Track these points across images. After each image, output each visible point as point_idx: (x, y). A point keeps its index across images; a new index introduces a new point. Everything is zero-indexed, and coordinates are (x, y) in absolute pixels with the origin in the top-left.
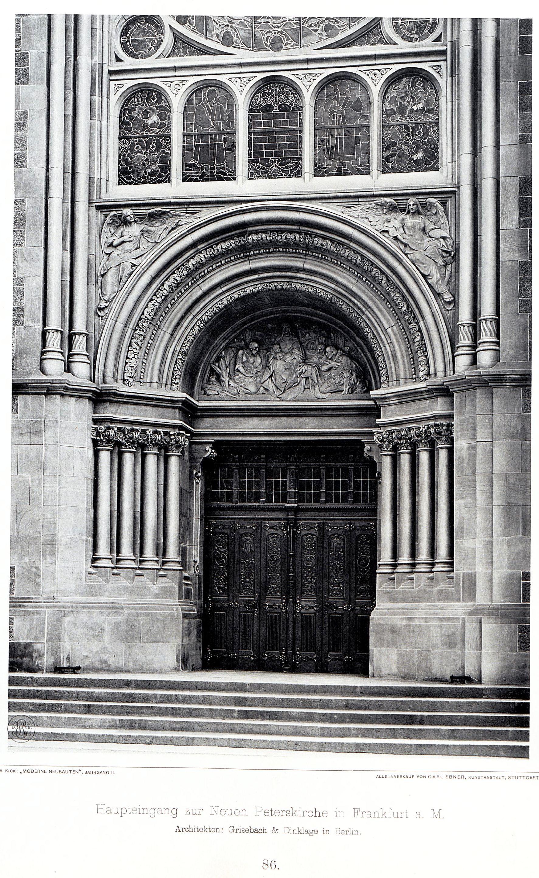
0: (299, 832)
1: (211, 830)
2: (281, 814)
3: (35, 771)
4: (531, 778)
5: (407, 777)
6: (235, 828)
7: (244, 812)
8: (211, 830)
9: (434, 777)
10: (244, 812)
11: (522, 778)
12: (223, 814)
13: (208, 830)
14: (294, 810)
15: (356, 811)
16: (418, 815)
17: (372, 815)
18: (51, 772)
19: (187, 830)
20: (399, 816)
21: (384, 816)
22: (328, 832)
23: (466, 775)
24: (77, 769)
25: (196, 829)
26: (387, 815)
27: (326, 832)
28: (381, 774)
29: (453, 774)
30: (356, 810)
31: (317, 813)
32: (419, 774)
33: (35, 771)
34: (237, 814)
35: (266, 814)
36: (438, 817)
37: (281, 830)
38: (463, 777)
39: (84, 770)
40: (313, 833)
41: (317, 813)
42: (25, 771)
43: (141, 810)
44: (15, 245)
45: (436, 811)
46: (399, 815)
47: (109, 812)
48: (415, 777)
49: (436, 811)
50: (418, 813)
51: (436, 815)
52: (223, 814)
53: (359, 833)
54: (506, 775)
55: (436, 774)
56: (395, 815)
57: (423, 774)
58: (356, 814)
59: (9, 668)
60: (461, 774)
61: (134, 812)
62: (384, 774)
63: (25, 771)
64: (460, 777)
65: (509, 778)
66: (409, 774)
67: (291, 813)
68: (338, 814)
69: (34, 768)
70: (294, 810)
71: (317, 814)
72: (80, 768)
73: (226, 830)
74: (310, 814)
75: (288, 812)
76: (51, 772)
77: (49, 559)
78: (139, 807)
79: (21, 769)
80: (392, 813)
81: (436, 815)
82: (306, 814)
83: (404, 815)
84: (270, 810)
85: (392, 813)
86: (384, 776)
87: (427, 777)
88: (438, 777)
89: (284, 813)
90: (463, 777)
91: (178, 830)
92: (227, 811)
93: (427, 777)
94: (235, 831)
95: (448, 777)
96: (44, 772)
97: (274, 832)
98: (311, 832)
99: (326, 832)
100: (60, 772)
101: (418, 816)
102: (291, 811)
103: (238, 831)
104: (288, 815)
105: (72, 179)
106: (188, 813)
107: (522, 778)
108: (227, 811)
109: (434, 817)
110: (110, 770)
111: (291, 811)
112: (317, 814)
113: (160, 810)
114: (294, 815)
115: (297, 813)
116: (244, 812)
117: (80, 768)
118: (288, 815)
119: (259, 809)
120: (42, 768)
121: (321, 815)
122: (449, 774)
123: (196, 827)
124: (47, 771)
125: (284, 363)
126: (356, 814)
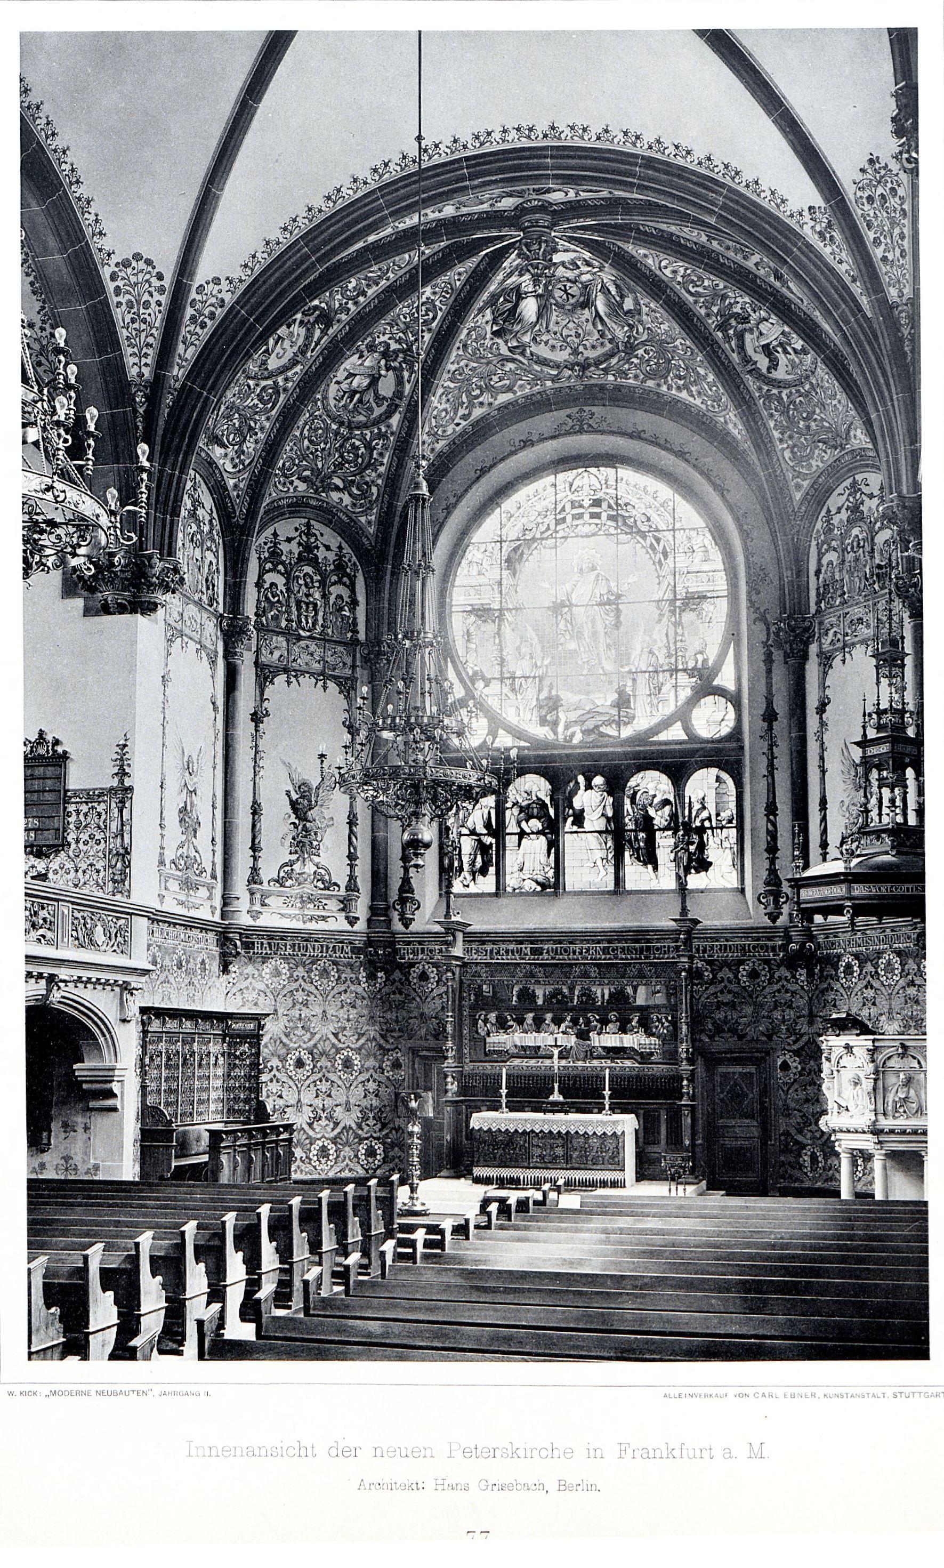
2: (492, 1454)
5: (717, 1396)
9: (764, 1395)
11: (917, 1395)
13: (414, 1486)
16: (728, 1453)
23: (780, 1392)
24: (145, 1388)
29: (796, 1391)
31: (303, 1450)
38: (813, 1395)
41: (303, 1450)
44: (35, 850)
45: (756, 1447)
46: (698, 1455)
49: (756, 1447)
59: (29, 1230)
60: (809, 1391)
61: (226, 1454)
63: (54, 1393)
66: (721, 1391)
68: (592, 1452)
71: (303, 1452)
72: (150, 1386)
74: (544, 1453)
77: (80, 1135)
79: (46, 1390)
81: (756, 1453)
82: (535, 1453)
83: (706, 1454)
89: (498, 1453)
90: (813, 1395)
93: (751, 1396)
103: (495, 1488)
107: (917, 1395)
112: (556, 1453)
117: (150, 1386)
122: (789, 1391)
124: (93, 1393)
125: (647, 638)
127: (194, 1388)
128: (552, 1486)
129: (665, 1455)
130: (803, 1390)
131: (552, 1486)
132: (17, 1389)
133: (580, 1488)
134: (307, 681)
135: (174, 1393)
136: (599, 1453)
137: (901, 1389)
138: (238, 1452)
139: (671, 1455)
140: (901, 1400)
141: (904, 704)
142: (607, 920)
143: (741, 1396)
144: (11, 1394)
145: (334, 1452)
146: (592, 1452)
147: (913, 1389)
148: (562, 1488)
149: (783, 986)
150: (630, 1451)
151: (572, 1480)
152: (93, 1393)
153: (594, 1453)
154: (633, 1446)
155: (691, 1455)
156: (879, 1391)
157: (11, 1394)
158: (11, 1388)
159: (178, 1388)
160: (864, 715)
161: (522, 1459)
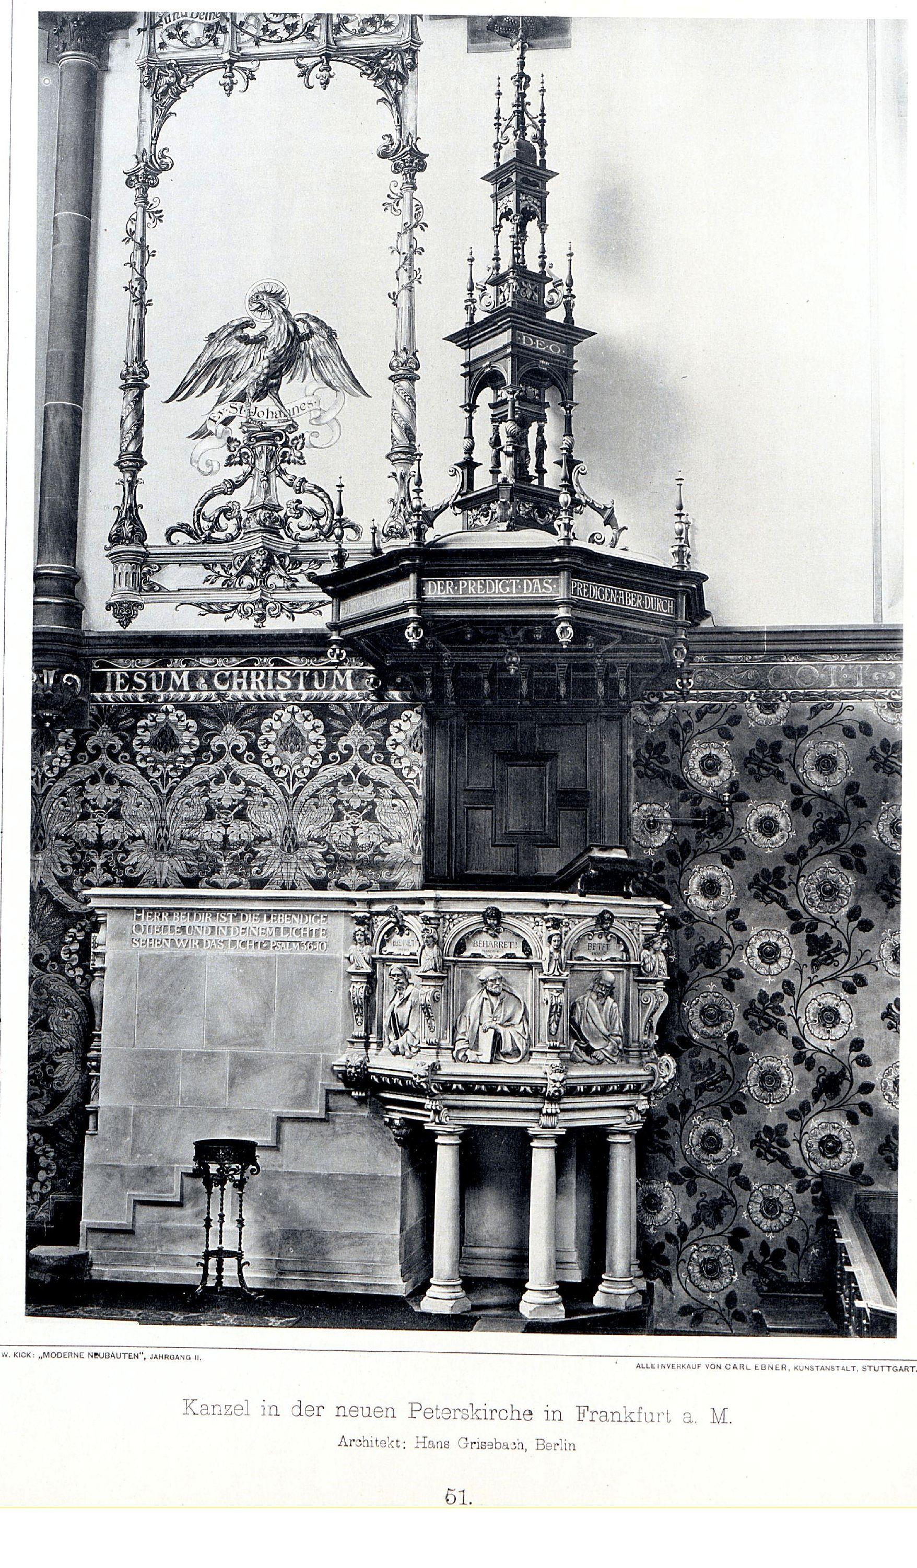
2: (316, 1412)
5: (689, 1366)
6: (469, 1441)
10: (390, 1411)
12: (378, 1415)
13: (394, 1444)
15: (582, 1411)
17: (210, 1410)
20: (551, 1417)
21: (628, 1419)
23: (751, 1363)
24: (136, 1351)
26: (635, 1417)
28: (643, 1361)
29: (767, 1362)
30: (583, 1411)
31: (516, 1413)
34: (310, 1413)
38: (784, 1367)
39: (148, 1353)
42: (46, 1355)
43: (489, 1413)
45: (719, 1412)
46: (489, 1416)
47: (204, 1412)
48: (703, 1367)
49: (719, 1412)
50: (687, 1415)
51: (720, 1418)
55: (738, 1362)
56: (649, 1418)
58: (582, 1415)
60: (780, 1362)
61: (238, 1412)
62: (650, 1361)
63: (46, 1355)
65: (864, 1369)
67: (470, 1413)
69: (62, 1350)
72: (141, 1350)
75: (465, 1412)
78: (485, 1407)
79: (39, 1351)
80: (642, 1416)
81: (720, 1418)
86: (649, 1366)
87: (193, 1358)
91: (343, 1444)
92: (360, 1410)
93: (193, 1358)
94: (469, 1446)
95: (760, 1368)
103: (475, 1446)
106: (229, 1412)
108: (360, 1410)
113: (604, 1414)
116: (390, 1411)
117: (141, 1350)
121: (371, 1414)
122: (759, 1363)
124: (85, 1355)
126: (582, 1415)
128: (531, 1445)
129: (623, 1418)
130: (774, 1363)
131: (531, 1445)
132: (11, 1351)
134: (139, 475)
136: (557, 1415)
137: (870, 1363)
138: (366, 1411)
139: (629, 1418)
140: (870, 1374)
141: (543, 265)
143: (712, 1367)
144: (5, 1355)
145: (297, 1411)
146: (551, 1414)
147: (870, 1363)
149: (228, 768)
150: (588, 1415)
151: (551, 1439)
152: (85, 1355)
153: (556, 1416)
155: (649, 1419)
156: (849, 1364)
159: (169, 1352)
160: (471, 289)
161: (515, 1421)
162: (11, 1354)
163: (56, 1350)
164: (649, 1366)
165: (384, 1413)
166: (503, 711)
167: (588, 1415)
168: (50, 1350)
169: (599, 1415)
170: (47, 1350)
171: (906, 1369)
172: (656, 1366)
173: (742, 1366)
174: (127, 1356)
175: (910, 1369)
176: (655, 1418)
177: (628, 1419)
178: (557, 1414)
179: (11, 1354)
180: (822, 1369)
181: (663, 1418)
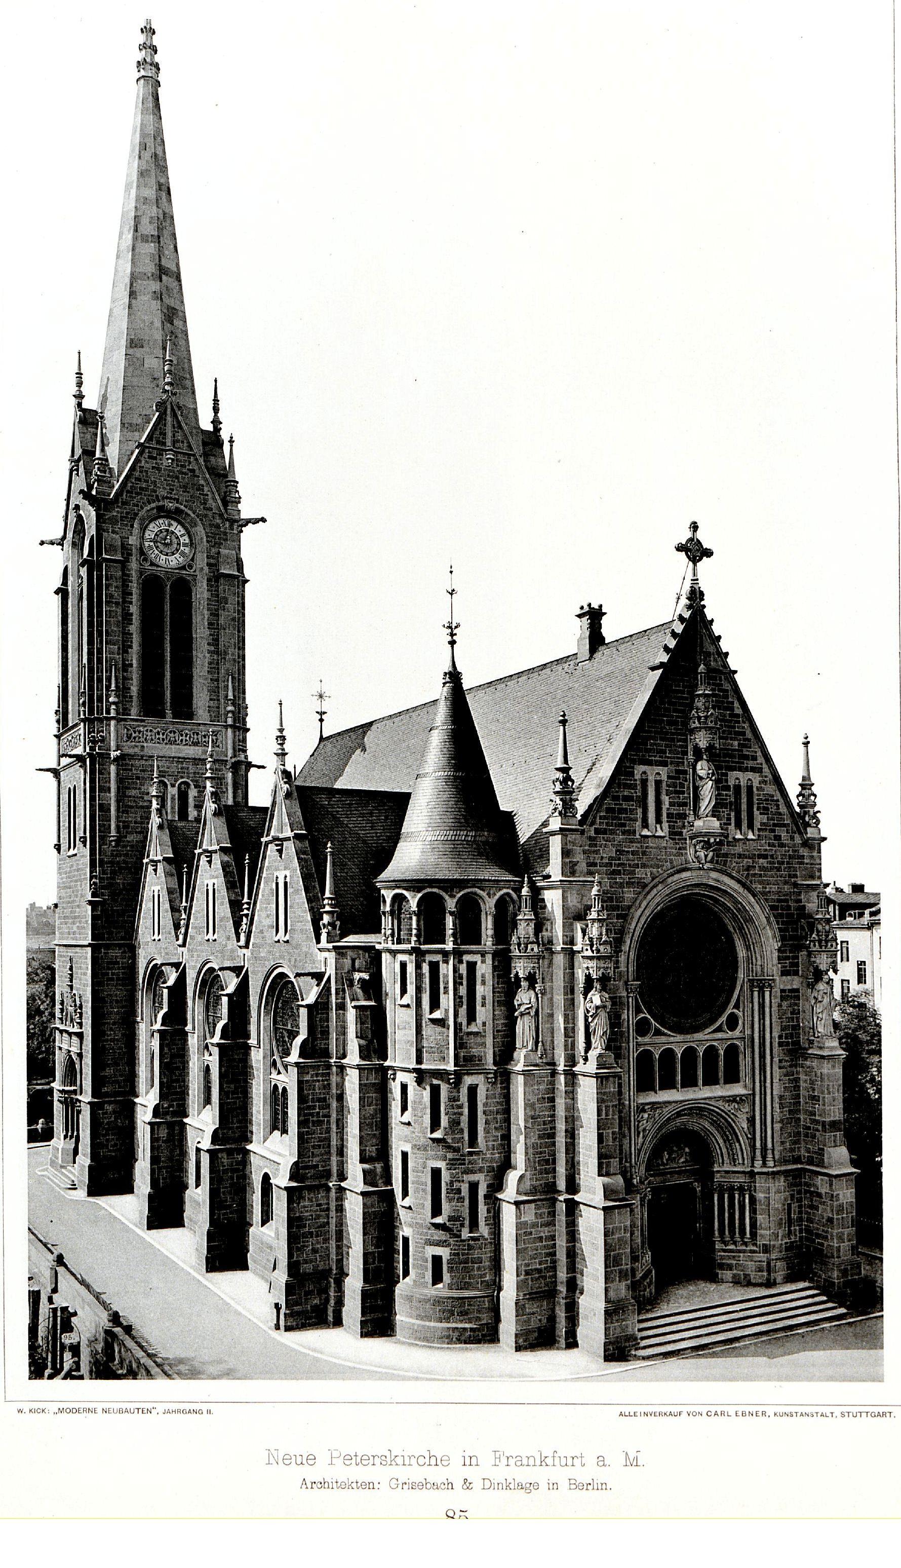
0: (508, 1487)
1: (359, 1484)
3: (78, 1411)
4: (879, 1414)
6: (400, 1482)
7: (311, 1459)
8: (359, 1484)
11: (864, 1415)
13: (354, 1485)
14: (394, 1454)
15: (497, 1456)
18: (105, 1411)
19: (319, 1486)
20: (468, 1463)
21: (393, 1463)
22: (604, 1486)
23: (770, 1411)
25: (335, 1484)
26: (549, 1461)
27: (554, 1486)
28: (626, 1409)
29: (747, 1409)
31: (433, 1459)
32: (691, 1409)
33: (78, 1411)
35: (347, 1462)
36: (635, 1463)
37: (477, 1484)
38: (764, 1413)
39: (161, 1408)
40: (532, 1488)
42: (61, 1411)
43: (407, 1459)
48: (684, 1415)
50: (601, 1459)
52: (287, 1462)
53: (608, 1488)
54: (837, 1411)
55: (719, 1409)
57: (697, 1409)
58: (498, 1460)
60: (760, 1409)
61: (364, 1462)
62: (632, 1409)
63: (61, 1411)
64: (760, 1414)
65: (843, 1415)
67: (388, 1459)
69: (77, 1405)
70: (394, 1454)
71: (433, 1461)
73: (384, 1486)
74: (421, 1460)
75: (383, 1458)
76: (105, 1411)
79: (54, 1407)
80: (557, 1460)
82: (413, 1461)
84: (353, 1454)
85: (557, 1460)
86: (632, 1414)
87: (205, 1412)
88: (722, 1413)
90: (764, 1413)
93: (205, 1412)
94: (400, 1486)
95: (760, 1414)
96: (94, 1411)
97: (465, 1487)
98: (532, 1486)
99: (554, 1486)
100: (120, 1411)
101: (601, 1463)
102: (388, 1457)
103: (406, 1487)
104: (384, 1463)
105: (67, 662)
107: (864, 1415)
108: (294, 1458)
109: (628, 1463)
110: (204, 1407)
111: (388, 1457)
113: (519, 1458)
114: (543, 1463)
115: (399, 1460)
117: (155, 1405)
118: (384, 1463)
119: (335, 1454)
120: (91, 1406)
121: (439, 1463)
122: (741, 1409)
123: (334, 1481)
124: (99, 1410)
127: (196, 1407)
129: (538, 1463)
130: (753, 1409)
132: (26, 1407)
133: (590, 1487)
135: (179, 1411)
142: (633, 697)
144: (20, 1411)
148: (573, 1487)
152: (99, 1410)
154: (507, 1454)
156: (827, 1410)
157: (20, 1411)
158: (20, 1406)
162: (26, 1410)
163: (71, 1405)
164: (632, 1414)
165: (371, 1461)
166: (202, 482)
167: (504, 1460)
168: (65, 1405)
169: (515, 1460)
170: (61, 1405)
171: (884, 1414)
172: (638, 1414)
173: (722, 1413)
174: (140, 1411)
175: (888, 1415)
176: (570, 1462)
177: (393, 1463)
178: (474, 1459)
179: (26, 1410)
180: (802, 1415)
181: (577, 1462)
